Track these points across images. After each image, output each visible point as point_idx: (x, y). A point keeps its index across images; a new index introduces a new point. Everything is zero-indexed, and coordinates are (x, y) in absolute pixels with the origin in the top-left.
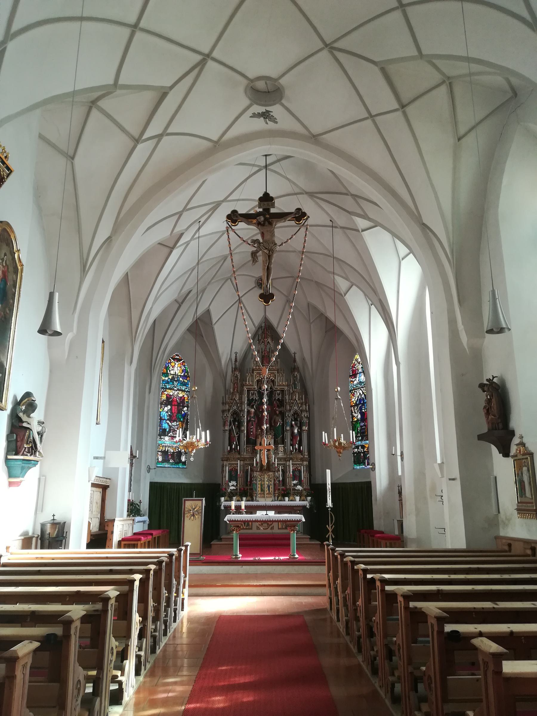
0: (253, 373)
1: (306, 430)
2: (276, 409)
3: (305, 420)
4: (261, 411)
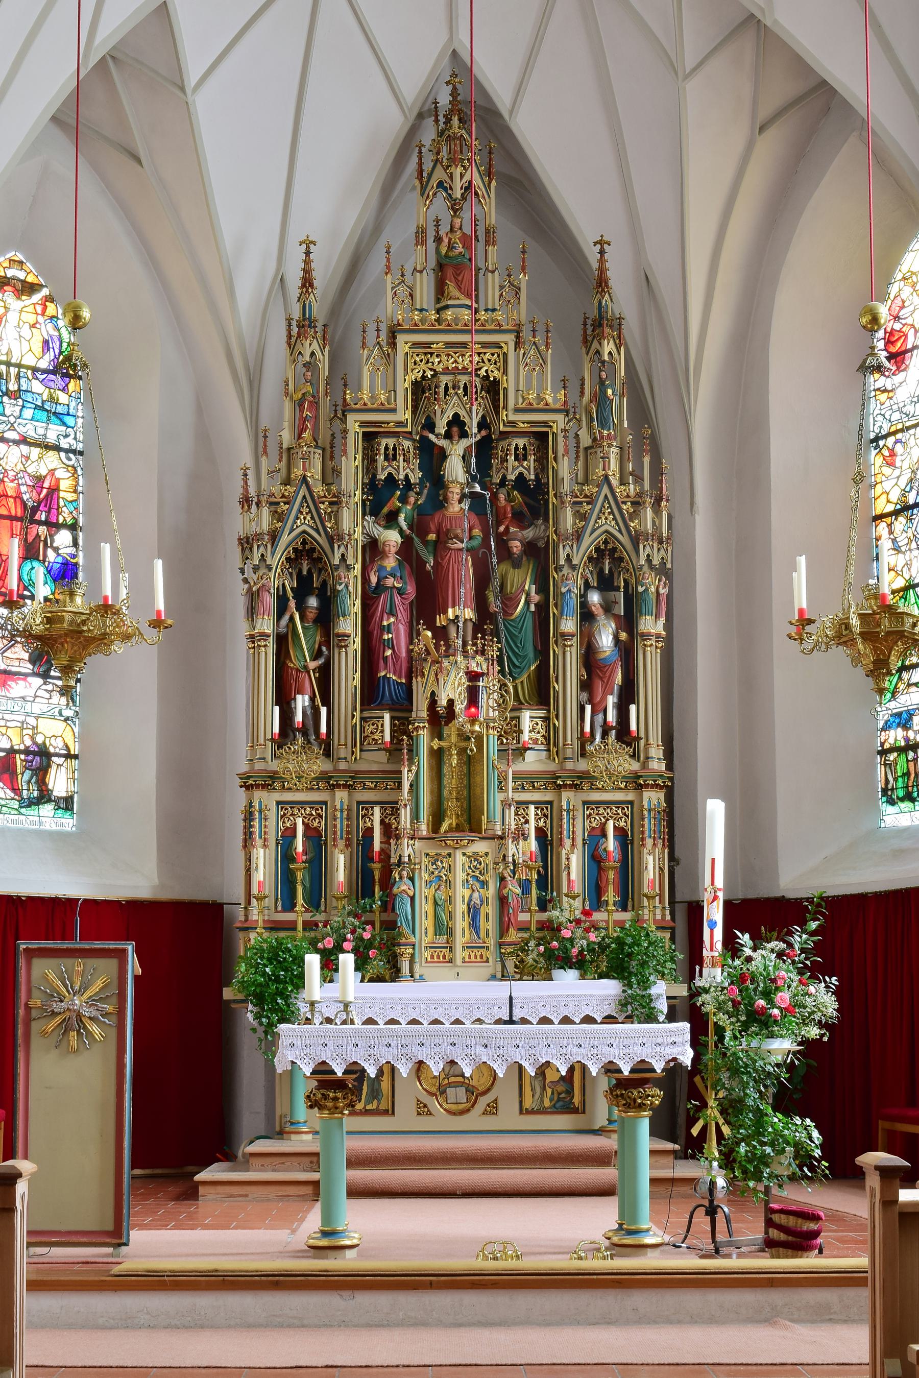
0: (393, 344)
1: (658, 636)
2: (507, 529)
3: (651, 584)
4: (436, 543)
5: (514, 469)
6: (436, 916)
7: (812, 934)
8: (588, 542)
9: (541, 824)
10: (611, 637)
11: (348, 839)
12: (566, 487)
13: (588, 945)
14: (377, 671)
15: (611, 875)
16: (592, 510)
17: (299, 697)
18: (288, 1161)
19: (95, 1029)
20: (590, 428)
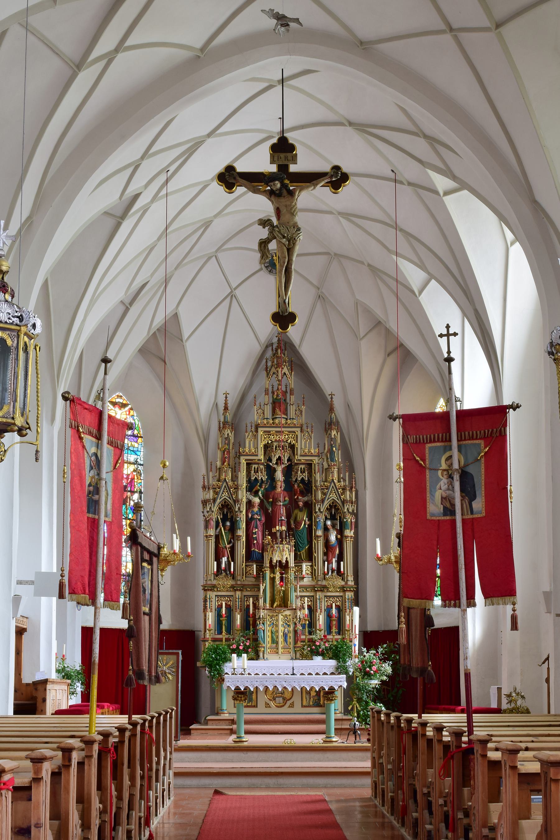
0: (257, 431)
1: (351, 537)
2: (298, 497)
3: (349, 519)
4: (272, 502)
5: (300, 476)
6: (272, 637)
7: (386, 648)
8: (326, 504)
9: (310, 603)
10: (335, 537)
11: (241, 609)
12: (318, 484)
13: (325, 648)
14: (251, 549)
15: (334, 623)
16: (328, 492)
17: (223, 559)
18: (221, 722)
19: (170, 676)
20: (327, 461)
